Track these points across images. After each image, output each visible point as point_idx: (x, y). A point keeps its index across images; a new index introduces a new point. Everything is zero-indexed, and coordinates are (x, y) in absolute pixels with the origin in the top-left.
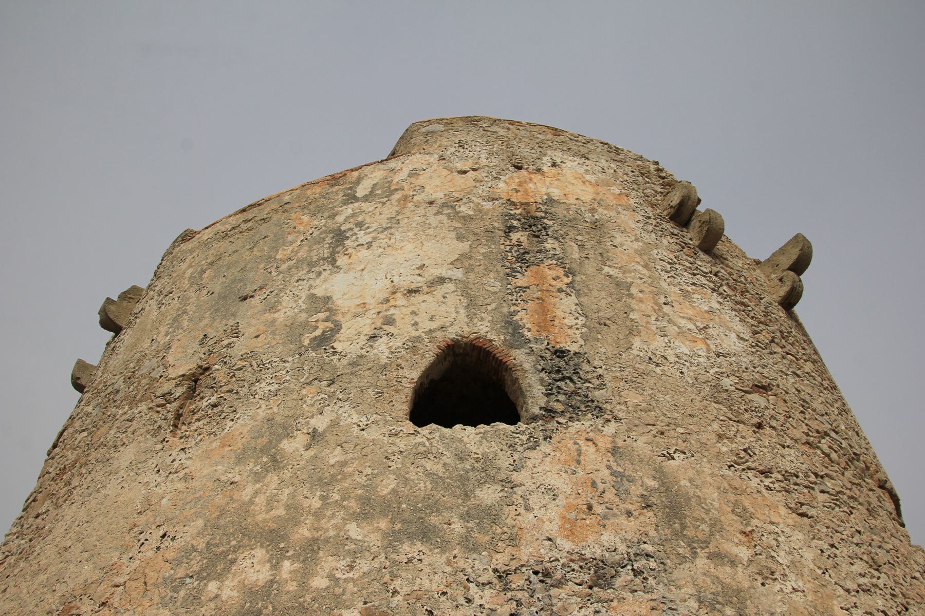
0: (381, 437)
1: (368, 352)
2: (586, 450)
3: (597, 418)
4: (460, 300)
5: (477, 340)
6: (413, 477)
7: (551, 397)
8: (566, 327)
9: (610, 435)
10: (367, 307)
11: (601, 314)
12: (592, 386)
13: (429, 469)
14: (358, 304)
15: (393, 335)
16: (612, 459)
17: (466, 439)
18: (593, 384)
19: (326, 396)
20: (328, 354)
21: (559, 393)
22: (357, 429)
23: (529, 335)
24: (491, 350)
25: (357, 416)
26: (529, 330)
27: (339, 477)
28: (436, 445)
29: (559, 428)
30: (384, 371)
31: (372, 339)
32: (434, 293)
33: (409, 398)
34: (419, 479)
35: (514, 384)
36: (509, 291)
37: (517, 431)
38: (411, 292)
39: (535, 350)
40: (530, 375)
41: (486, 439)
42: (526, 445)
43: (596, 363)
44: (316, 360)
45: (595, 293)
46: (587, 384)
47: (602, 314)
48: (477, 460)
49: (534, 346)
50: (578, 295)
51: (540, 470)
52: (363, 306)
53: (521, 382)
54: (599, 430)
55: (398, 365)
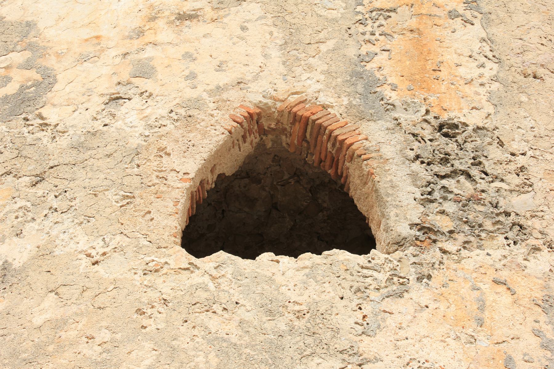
0: (130, 275)
1: (105, 125)
2: (494, 301)
3: (515, 243)
4: (271, 33)
5: (301, 106)
6: (186, 346)
7: (432, 205)
8: (462, 82)
9: (540, 275)
10: (104, 44)
11: (529, 57)
12: (507, 187)
13: (213, 331)
14: (86, 37)
15: (151, 95)
16: (543, 318)
17: (279, 278)
18: (509, 184)
19: (29, 204)
20: (31, 128)
21: (445, 199)
22: (85, 262)
23: (393, 96)
24: (325, 124)
25: (86, 238)
26: (394, 88)
27: (51, 348)
28: (226, 288)
29: (445, 261)
30: (136, 158)
31: (113, 104)
32: (225, 20)
33: (180, 207)
34: (196, 349)
35: (366, 183)
36: (360, 17)
37: (369, 265)
38: (183, 17)
39: (404, 124)
40: (394, 167)
41: (314, 278)
42: (386, 290)
43: (515, 147)
44: (9, 139)
45: (520, 18)
46: (497, 184)
47: (530, 56)
48: (299, 315)
49: (402, 116)
50: (487, 21)
51: (410, 334)
52: (95, 41)
53: (377, 179)
54: (518, 265)
55: (160, 149)
